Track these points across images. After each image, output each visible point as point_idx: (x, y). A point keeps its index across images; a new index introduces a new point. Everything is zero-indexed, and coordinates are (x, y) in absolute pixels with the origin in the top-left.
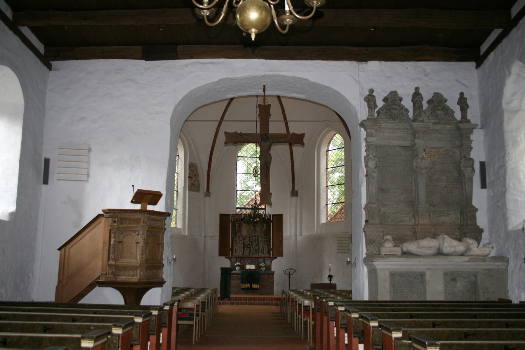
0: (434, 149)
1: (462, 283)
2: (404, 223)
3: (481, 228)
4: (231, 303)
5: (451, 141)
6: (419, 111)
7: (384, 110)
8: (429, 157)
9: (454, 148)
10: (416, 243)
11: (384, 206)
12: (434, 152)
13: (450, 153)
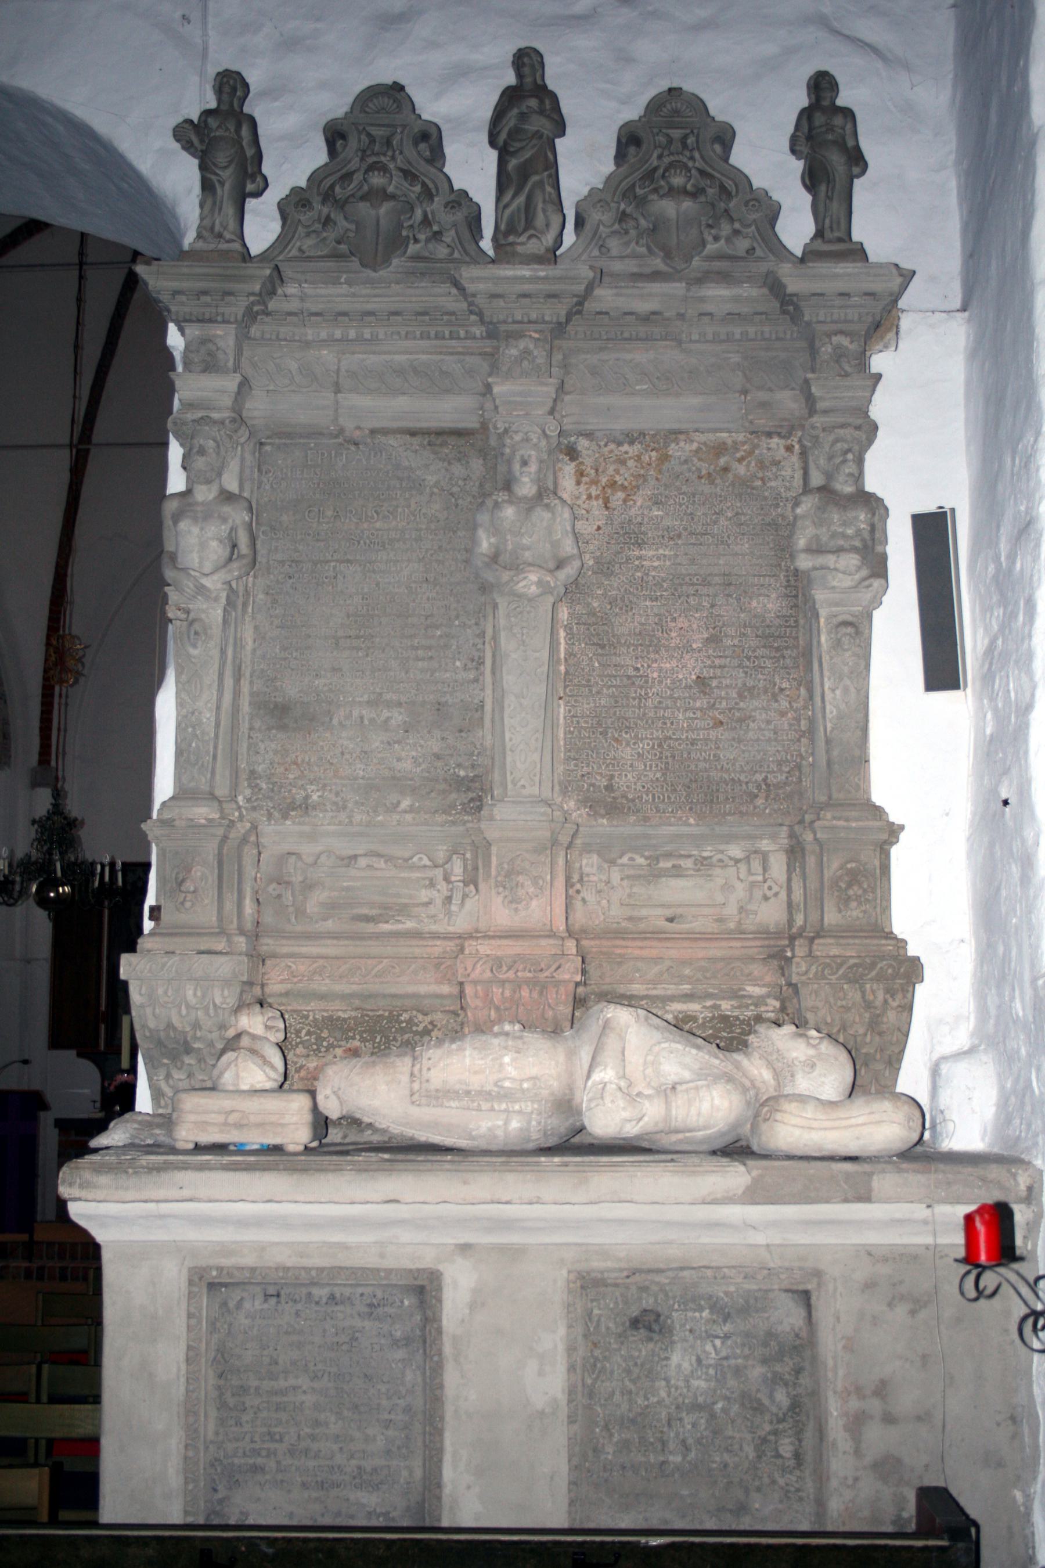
0: (631, 443)
1: (709, 1347)
2: (410, 925)
3: (912, 951)
4: (28, 1274)
5: (745, 392)
6: (521, 199)
7: (312, 208)
8: (597, 497)
9: (769, 435)
10: (403, 1065)
11: (285, 816)
12: (631, 463)
13: (741, 470)
